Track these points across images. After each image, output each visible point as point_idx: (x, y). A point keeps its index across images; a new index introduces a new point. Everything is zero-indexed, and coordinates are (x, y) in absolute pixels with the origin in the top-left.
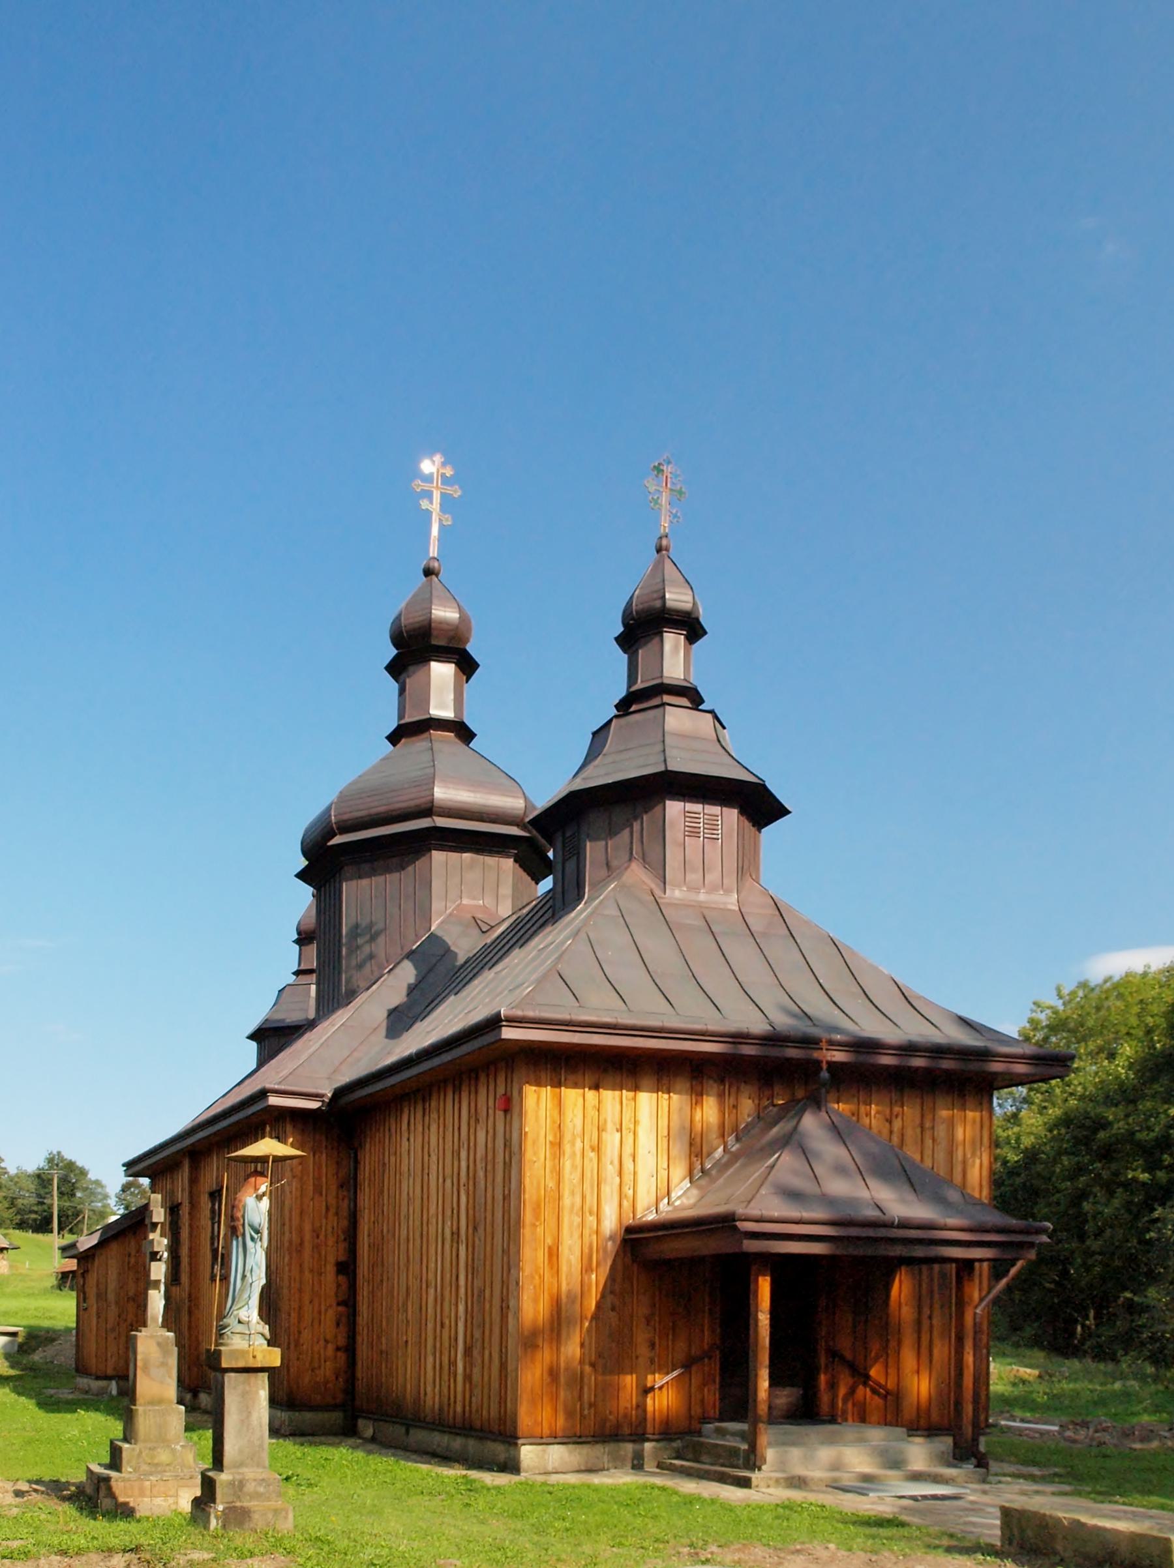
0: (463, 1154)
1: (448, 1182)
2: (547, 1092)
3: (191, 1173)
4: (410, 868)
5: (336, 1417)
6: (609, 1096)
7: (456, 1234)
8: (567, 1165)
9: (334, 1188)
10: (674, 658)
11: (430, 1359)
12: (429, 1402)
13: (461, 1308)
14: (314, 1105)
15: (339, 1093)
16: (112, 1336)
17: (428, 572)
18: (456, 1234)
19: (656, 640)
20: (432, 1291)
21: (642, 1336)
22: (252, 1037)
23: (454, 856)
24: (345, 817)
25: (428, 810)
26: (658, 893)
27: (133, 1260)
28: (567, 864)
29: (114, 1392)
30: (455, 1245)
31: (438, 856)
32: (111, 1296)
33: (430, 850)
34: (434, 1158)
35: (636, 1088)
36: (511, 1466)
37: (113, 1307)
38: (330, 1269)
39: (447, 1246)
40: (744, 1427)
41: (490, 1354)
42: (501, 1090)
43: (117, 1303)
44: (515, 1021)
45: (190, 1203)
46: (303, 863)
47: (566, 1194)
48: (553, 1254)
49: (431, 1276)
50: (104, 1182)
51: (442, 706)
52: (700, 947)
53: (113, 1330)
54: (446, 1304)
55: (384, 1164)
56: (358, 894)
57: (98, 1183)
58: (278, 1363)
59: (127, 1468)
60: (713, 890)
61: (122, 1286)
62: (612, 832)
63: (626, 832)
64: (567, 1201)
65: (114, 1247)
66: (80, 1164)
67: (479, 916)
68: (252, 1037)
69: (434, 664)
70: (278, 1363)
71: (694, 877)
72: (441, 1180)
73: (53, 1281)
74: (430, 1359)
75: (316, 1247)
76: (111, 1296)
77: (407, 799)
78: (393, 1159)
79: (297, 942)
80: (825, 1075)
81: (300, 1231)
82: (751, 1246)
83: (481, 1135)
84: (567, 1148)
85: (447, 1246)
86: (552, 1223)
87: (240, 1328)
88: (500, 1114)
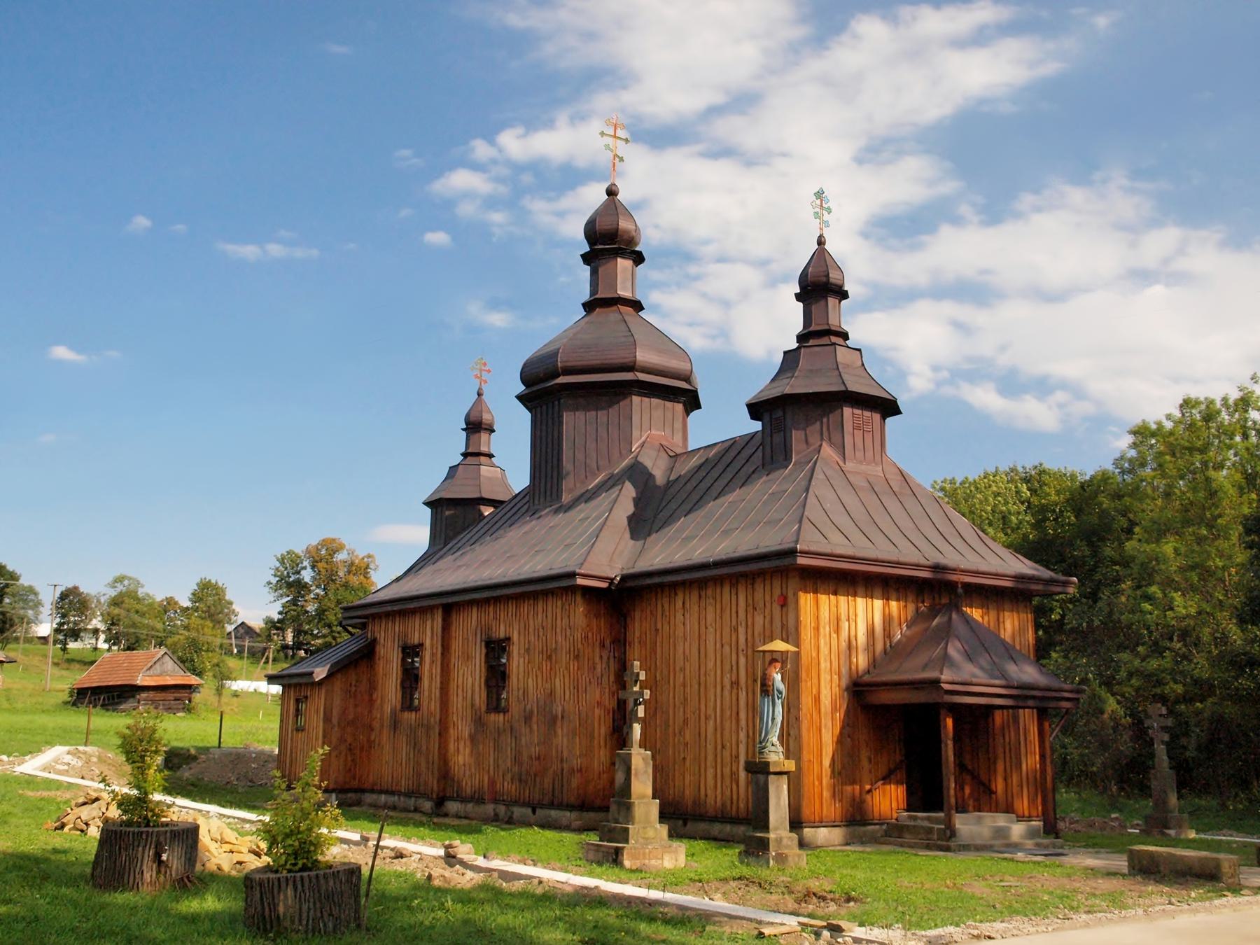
0: (741, 630)
1: (727, 648)
2: (810, 596)
3: (444, 620)
4: (616, 407)
6: (842, 599)
7: (735, 684)
8: (822, 642)
11: (710, 772)
12: (710, 800)
13: (742, 735)
14: (604, 585)
15: (625, 578)
18: (735, 684)
19: (822, 302)
20: (711, 723)
21: (864, 754)
22: (427, 504)
24: (569, 364)
25: (631, 368)
26: (841, 463)
27: (353, 689)
28: (775, 436)
30: (735, 691)
31: (636, 399)
33: (631, 394)
34: (711, 630)
35: (855, 595)
39: (726, 693)
40: (942, 815)
42: (777, 592)
44: (806, 553)
45: (443, 646)
46: (521, 388)
47: (822, 661)
48: (817, 700)
49: (710, 712)
50: (38, 589)
51: (624, 289)
52: (872, 501)
54: (727, 733)
55: (657, 630)
57: (31, 590)
58: (794, 769)
59: (632, 841)
60: (868, 464)
61: (344, 712)
62: (809, 422)
64: (823, 665)
66: (10, 568)
67: (664, 443)
69: (619, 260)
70: (794, 769)
71: (860, 454)
72: (718, 645)
73: (66, 697)
74: (710, 772)
77: (617, 357)
78: (666, 627)
80: (960, 590)
82: (948, 698)
83: (759, 620)
84: (822, 630)
85: (726, 693)
86: (815, 681)
87: (773, 749)
88: (777, 608)
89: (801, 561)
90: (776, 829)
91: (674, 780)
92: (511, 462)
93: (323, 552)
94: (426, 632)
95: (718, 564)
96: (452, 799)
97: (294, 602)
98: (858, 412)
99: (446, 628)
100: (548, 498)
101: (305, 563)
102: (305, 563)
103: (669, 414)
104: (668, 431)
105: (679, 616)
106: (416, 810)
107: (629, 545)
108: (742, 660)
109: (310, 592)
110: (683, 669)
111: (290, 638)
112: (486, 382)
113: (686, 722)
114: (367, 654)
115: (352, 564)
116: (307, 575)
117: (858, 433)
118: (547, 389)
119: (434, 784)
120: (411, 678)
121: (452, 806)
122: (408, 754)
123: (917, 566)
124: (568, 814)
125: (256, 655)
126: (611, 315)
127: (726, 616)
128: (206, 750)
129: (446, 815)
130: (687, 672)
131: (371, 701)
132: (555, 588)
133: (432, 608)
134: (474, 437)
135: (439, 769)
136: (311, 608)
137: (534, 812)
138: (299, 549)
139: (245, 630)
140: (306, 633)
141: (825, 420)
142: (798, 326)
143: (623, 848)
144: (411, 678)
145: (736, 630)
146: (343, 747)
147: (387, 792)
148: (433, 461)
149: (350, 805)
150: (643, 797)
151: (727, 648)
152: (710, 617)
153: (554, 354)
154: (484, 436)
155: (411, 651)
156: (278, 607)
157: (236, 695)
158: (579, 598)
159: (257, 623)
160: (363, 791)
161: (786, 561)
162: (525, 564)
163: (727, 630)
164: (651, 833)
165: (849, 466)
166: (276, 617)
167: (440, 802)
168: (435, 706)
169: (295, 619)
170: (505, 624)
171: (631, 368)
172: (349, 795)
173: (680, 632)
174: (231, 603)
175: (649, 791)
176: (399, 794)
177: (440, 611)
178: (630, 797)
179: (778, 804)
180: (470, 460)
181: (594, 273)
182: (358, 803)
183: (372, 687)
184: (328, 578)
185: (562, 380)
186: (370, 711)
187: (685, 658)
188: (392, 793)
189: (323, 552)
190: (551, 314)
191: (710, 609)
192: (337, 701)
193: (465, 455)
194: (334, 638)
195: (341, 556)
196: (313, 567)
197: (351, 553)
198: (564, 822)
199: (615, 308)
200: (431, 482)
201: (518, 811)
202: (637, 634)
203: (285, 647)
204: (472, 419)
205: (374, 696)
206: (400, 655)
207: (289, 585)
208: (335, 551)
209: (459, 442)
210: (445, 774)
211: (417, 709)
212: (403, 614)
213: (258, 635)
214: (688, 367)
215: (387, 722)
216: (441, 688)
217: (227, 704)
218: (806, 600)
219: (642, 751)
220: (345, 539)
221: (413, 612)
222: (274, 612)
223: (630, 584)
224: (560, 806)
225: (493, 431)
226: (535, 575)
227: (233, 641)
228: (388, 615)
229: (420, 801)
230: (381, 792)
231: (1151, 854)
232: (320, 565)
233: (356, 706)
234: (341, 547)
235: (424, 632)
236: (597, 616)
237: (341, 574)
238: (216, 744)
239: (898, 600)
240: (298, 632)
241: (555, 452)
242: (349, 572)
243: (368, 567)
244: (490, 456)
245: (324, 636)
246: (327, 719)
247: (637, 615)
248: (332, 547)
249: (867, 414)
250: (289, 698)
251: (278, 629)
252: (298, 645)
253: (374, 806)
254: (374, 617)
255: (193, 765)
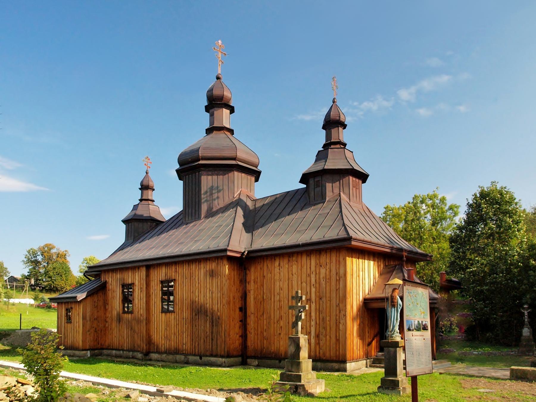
0: (313, 276)
1: (304, 284)
4: (227, 176)
5: (239, 359)
9: (238, 282)
10: (225, 117)
13: (313, 323)
15: (249, 252)
16: (88, 333)
17: (218, 78)
19: (337, 128)
22: (124, 221)
23: (240, 174)
24: (205, 155)
25: (234, 159)
29: (89, 356)
31: (236, 173)
32: (88, 318)
36: (345, 370)
37: (89, 322)
38: (237, 310)
41: (330, 337)
43: (90, 320)
45: (146, 284)
53: (89, 331)
55: (264, 277)
56: (207, 181)
61: (92, 314)
63: (338, 183)
65: (89, 298)
68: (124, 221)
72: (299, 283)
75: (234, 302)
76: (88, 318)
79: (140, 189)
81: (229, 297)
83: (323, 271)
89: (229, 253)
90: (400, 375)
91: (274, 343)
92: (168, 203)
93: (46, 249)
94: (137, 278)
95: (304, 245)
96: (152, 352)
97: (34, 268)
98: (354, 179)
99: (148, 276)
100: (190, 218)
101: (39, 253)
102: (39, 253)
103: (249, 181)
104: (249, 189)
105: (277, 270)
106: (133, 357)
107: (246, 236)
108: (313, 290)
109: (41, 264)
110: (279, 294)
111: (33, 282)
112: (149, 167)
113: (281, 317)
114: (103, 288)
115: (59, 254)
116: (40, 258)
117: (354, 189)
118: (191, 168)
119: (145, 347)
120: (127, 299)
121: (154, 356)
122: (127, 333)
123: (383, 246)
124: (221, 359)
125: (21, 288)
126: (221, 135)
127: (304, 270)
128: (14, 331)
129: (150, 360)
130: (282, 295)
131: (106, 310)
132: (218, 255)
133: (139, 267)
134: (145, 192)
135: (146, 339)
136: (42, 271)
137: (201, 358)
138: (36, 248)
139: (12, 279)
140: (40, 280)
141: (341, 181)
142: (323, 142)
143: (279, 381)
144: (127, 299)
145: (310, 276)
146: (92, 330)
147: (116, 350)
148: (127, 203)
149: (96, 356)
150: (304, 358)
151: (304, 284)
152: (294, 270)
153: (198, 150)
154: (150, 192)
155: (127, 286)
156: (27, 270)
157: (13, 304)
158: (225, 262)
159: (18, 276)
160: (103, 349)
161: (346, 243)
162: (192, 246)
163: (304, 276)
164: (310, 376)
165: (351, 203)
166: (27, 274)
167: (147, 354)
168: (143, 312)
169: (35, 275)
170: (180, 274)
171: (234, 159)
172: (96, 351)
173: (277, 277)
174: (6, 269)
175: (307, 356)
176: (123, 350)
177: (144, 268)
178: (299, 358)
179: (400, 362)
180: (143, 202)
181: (212, 115)
182: (101, 354)
183: (106, 303)
184: (49, 259)
185: (201, 162)
186: (105, 314)
187: (281, 289)
188: (119, 350)
189: (46, 249)
190: (191, 133)
191: (295, 267)
192: (88, 310)
193: (141, 200)
194: (53, 282)
195: (53, 251)
196: (42, 255)
197: (58, 249)
198: (219, 363)
199: (222, 132)
200: (126, 212)
201: (191, 358)
202: (252, 278)
203: (31, 286)
204: (144, 183)
205: (107, 307)
206: (121, 289)
207: (32, 262)
208: (50, 249)
209: (138, 194)
210: (149, 341)
211: (132, 313)
212: (122, 270)
213: (19, 281)
214: (257, 161)
215: (115, 319)
216: (146, 303)
217: (11, 309)
218: (349, 260)
219: (303, 335)
220: (55, 244)
221: (127, 269)
222: (26, 272)
223: (252, 255)
224: (216, 356)
225: (154, 190)
226: (190, 252)
227: (8, 283)
228: (113, 271)
229: (135, 353)
230: (113, 349)
231: (524, 371)
232: (45, 254)
233: (98, 311)
234: (53, 247)
235: (135, 278)
236: (234, 270)
237: (54, 258)
238: (19, 328)
239: (374, 260)
240: (36, 280)
241: (187, 201)
242: (58, 257)
243: (65, 255)
244: (153, 201)
245: (48, 281)
246: (84, 318)
247: (253, 269)
248: (50, 247)
249: (357, 180)
250: (62, 310)
251: (27, 278)
252: (37, 285)
253: (108, 355)
254: (105, 271)
255: (8, 338)
